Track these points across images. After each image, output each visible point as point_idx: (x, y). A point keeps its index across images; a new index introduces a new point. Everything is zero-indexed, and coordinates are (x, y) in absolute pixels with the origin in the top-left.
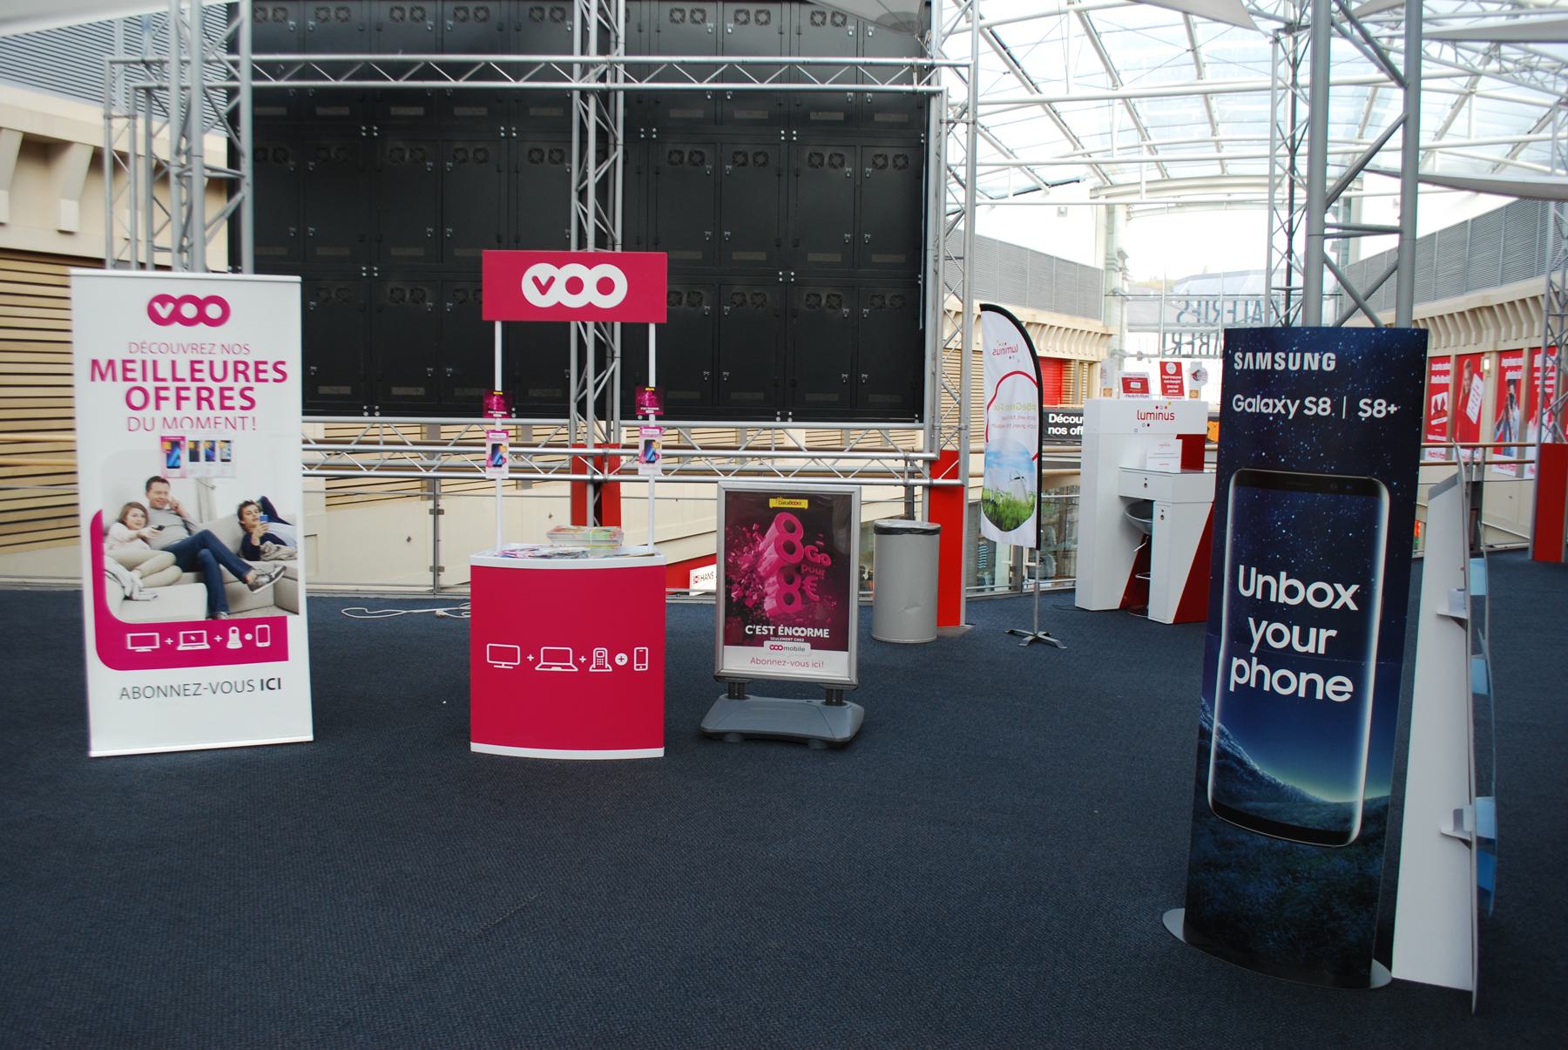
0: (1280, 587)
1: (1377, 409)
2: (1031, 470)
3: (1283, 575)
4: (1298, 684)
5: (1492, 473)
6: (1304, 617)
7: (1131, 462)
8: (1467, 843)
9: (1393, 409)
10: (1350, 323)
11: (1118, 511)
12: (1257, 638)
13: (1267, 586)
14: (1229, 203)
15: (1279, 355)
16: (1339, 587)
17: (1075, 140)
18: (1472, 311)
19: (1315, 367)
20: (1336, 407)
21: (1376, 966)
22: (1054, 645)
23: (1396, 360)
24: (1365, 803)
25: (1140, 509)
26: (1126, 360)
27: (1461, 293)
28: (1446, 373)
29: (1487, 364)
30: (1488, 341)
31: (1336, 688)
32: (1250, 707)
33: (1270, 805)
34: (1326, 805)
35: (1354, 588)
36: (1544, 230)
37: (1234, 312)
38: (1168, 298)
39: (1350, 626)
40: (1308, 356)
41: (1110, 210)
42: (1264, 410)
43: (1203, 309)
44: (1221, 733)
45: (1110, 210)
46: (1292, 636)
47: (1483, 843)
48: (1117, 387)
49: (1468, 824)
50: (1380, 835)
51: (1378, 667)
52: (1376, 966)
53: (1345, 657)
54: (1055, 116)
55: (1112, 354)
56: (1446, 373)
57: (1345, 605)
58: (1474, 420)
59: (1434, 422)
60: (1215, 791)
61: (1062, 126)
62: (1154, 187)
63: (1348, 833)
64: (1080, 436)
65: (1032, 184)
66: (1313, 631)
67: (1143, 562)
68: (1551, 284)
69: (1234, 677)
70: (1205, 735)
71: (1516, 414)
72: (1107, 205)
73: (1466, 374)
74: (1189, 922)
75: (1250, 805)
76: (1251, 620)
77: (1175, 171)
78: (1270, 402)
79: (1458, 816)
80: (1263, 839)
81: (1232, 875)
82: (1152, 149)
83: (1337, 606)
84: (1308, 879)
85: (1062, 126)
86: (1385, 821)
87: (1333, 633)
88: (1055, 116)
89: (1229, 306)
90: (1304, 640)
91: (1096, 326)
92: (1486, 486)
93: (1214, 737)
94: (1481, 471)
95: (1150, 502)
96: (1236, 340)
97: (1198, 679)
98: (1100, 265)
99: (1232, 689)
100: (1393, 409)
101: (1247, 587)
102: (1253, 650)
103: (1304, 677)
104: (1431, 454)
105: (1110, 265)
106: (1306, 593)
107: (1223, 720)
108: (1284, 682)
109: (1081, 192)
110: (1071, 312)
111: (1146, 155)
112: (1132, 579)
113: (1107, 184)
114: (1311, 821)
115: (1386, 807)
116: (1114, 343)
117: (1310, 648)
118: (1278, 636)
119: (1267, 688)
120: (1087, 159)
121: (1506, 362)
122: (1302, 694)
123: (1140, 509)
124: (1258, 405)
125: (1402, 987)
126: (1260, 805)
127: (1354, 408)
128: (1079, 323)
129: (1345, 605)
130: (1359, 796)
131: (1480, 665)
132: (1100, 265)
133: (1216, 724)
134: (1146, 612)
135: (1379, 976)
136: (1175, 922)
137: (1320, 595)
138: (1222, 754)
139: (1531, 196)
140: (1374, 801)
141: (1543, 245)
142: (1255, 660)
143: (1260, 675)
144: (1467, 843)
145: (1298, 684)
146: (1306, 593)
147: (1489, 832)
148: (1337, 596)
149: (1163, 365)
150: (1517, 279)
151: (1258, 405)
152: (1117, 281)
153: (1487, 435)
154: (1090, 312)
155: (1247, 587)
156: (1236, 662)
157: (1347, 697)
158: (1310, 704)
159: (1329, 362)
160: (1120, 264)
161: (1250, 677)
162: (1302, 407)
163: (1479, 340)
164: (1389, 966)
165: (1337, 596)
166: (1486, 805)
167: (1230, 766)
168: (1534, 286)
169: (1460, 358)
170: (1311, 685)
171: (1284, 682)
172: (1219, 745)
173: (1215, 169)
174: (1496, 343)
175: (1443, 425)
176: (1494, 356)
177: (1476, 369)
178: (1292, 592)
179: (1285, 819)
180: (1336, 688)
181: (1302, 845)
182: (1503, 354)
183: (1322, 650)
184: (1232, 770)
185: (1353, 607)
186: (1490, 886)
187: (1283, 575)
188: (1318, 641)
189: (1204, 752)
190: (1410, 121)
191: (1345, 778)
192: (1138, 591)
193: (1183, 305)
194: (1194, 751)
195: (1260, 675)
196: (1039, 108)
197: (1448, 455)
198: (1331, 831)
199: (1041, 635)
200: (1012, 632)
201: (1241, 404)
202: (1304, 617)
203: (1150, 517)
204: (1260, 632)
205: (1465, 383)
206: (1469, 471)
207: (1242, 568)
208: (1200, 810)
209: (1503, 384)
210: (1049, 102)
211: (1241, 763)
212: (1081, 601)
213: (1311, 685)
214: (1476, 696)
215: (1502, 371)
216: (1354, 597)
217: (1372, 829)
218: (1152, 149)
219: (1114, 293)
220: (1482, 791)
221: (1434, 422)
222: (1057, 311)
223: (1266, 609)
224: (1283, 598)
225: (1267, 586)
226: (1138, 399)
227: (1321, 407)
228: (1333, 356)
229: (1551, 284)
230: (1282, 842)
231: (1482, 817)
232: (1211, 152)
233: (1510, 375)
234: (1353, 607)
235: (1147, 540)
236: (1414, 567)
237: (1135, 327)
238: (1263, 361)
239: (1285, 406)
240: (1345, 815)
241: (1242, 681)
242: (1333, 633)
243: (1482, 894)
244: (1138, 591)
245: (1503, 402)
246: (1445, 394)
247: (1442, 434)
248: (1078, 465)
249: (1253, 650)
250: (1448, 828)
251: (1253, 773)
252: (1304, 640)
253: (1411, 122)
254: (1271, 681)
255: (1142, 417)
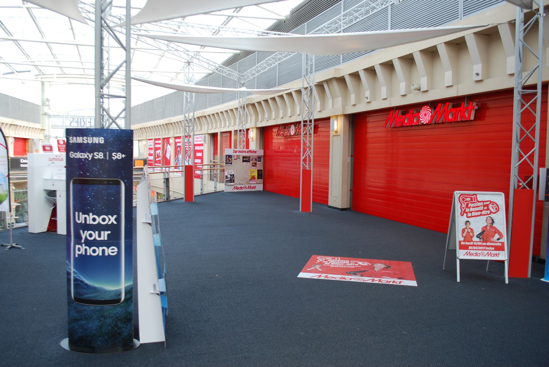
0: (90, 219)
1: (118, 156)
2: (5, 181)
3: (91, 214)
4: (99, 251)
5: (171, 175)
6: (99, 228)
7: (47, 176)
8: (158, 294)
9: (124, 156)
10: (111, 128)
11: (44, 195)
12: (84, 237)
13: (85, 218)
14: (87, 84)
15: (85, 138)
16: (110, 216)
17: (27, 56)
18: (166, 124)
19: (97, 142)
20: (105, 156)
21: (135, 340)
22: (19, 248)
23: (124, 140)
24: (125, 288)
25: (52, 194)
26: (51, 139)
27: (163, 118)
28: (159, 144)
29: (172, 141)
30: (171, 134)
31: (111, 251)
32: (84, 262)
33: (93, 295)
34: (112, 291)
35: (115, 216)
36: (183, 102)
37: (90, 122)
38: (66, 117)
39: (114, 229)
40: (94, 138)
41: (43, 83)
42: (81, 157)
43: (79, 121)
44: (75, 273)
45: (43, 83)
46: (95, 235)
47: (162, 293)
48: (41, 149)
49: (158, 289)
50: (131, 297)
51: (125, 242)
52: (135, 340)
53: (113, 240)
54: (19, 46)
55: (46, 137)
56: (159, 144)
57: (112, 223)
58: (169, 158)
59: (157, 159)
60: (74, 293)
61: (22, 50)
62: (59, 76)
63: (120, 299)
64: (26, 168)
65: (11, 71)
66: (102, 232)
67: (54, 213)
68: (185, 117)
69: (77, 252)
70: (69, 274)
71: (180, 156)
72: (41, 81)
73: (165, 144)
74: (70, 343)
75: (87, 296)
76: (81, 231)
77: (67, 71)
78: (83, 154)
79: (154, 286)
80: (92, 307)
81: (83, 322)
82: (58, 62)
83: (110, 223)
84: (109, 318)
85: (22, 50)
86: (132, 292)
87: (109, 232)
88: (19, 46)
89: (88, 120)
90: (100, 236)
91: (38, 126)
92: (170, 179)
93: (72, 275)
94: (169, 175)
95: (55, 191)
96: (70, 132)
97: (65, 253)
98: (40, 104)
99: (77, 256)
100: (124, 156)
101: (79, 219)
102: (83, 241)
103: (101, 248)
104: (157, 170)
105: (43, 104)
106: (99, 220)
107: (75, 268)
108: (94, 251)
109: (31, 76)
110: (28, 120)
111: (56, 65)
112: (51, 220)
113: (41, 73)
114: (108, 297)
115: (132, 288)
116: (46, 133)
117: (102, 238)
118: (91, 235)
119: (88, 254)
120: (33, 64)
121: (177, 140)
122: (101, 254)
123: (52, 194)
124: (78, 155)
125: (144, 346)
126: (90, 295)
127: (111, 156)
128: (32, 125)
129: (112, 223)
130: (123, 286)
131: (157, 237)
132: (40, 104)
133: (73, 269)
134: (56, 231)
135: (137, 343)
136: (65, 344)
137: (104, 220)
138: (76, 280)
139: (180, 90)
140: (128, 286)
141: (183, 105)
142: (84, 245)
143: (86, 250)
144: (158, 294)
145: (99, 251)
146: (99, 220)
147: (164, 290)
148: (110, 220)
149: (58, 141)
150: (178, 115)
151: (78, 155)
152: (46, 110)
153: (172, 163)
154: (37, 121)
155: (79, 219)
156: (77, 246)
157: (116, 253)
158: (104, 258)
159: (101, 140)
160: (47, 103)
161: (82, 252)
162: (94, 156)
163: (169, 133)
164: (138, 339)
165: (110, 220)
166: (162, 281)
167: (78, 284)
168: (180, 118)
169: (164, 139)
170: (103, 251)
171: (94, 251)
172: (74, 277)
173: (81, 72)
174: (207, 130)
175: (159, 161)
176: (173, 139)
177: (168, 143)
178: (94, 220)
179: (99, 298)
180: (111, 251)
181: (107, 306)
182: (176, 138)
183: (106, 239)
184: (79, 285)
185: (115, 223)
186: (166, 306)
187: (91, 214)
188: (105, 235)
189: (69, 280)
190: (128, 62)
191: (117, 280)
192: (53, 224)
193: (72, 119)
194: (66, 280)
195: (86, 250)
196: (12, 42)
197: (162, 170)
198: (116, 301)
199: (14, 245)
200: (2, 245)
201: (73, 155)
202: (99, 228)
203: (55, 196)
204: (85, 235)
205: (165, 147)
206: (165, 175)
207: (77, 213)
208: (70, 302)
209: (176, 147)
210: (16, 40)
211: (82, 282)
212: (31, 230)
213: (103, 251)
214: (156, 247)
215: (176, 143)
216: (116, 220)
217: (128, 296)
218: (58, 62)
219: (45, 114)
220: (160, 277)
221: (157, 159)
222: (22, 120)
223: (86, 227)
224: (92, 222)
225: (85, 218)
226: (49, 154)
227: (100, 156)
228: (103, 138)
229: (185, 117)
230: (99, 307)
231: (161, 286)
232: (80, 65)
233: (178, 144)
234: (115, 223)
235: (55, 205)
236: (134, 209)
237: (53, 127)
238: (79, 140)
239: (88, 156)
240: (119, 293)
241: (80, 253)
242: (109, 232)
243: (163, 309)
244: (53, 224)
245: (176, 153)
246: (159, 151)
247: (160, 163)
248: (26, 179)
249: (83, 241)
250: (152, 291)
251: (87, 285)
252: (100, 236)
253: (128, 62)
254: (90, 251)
255: (50, 160)
